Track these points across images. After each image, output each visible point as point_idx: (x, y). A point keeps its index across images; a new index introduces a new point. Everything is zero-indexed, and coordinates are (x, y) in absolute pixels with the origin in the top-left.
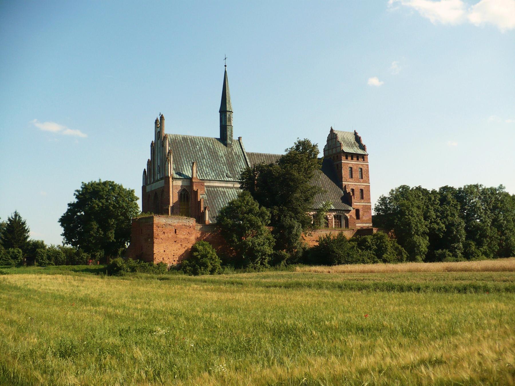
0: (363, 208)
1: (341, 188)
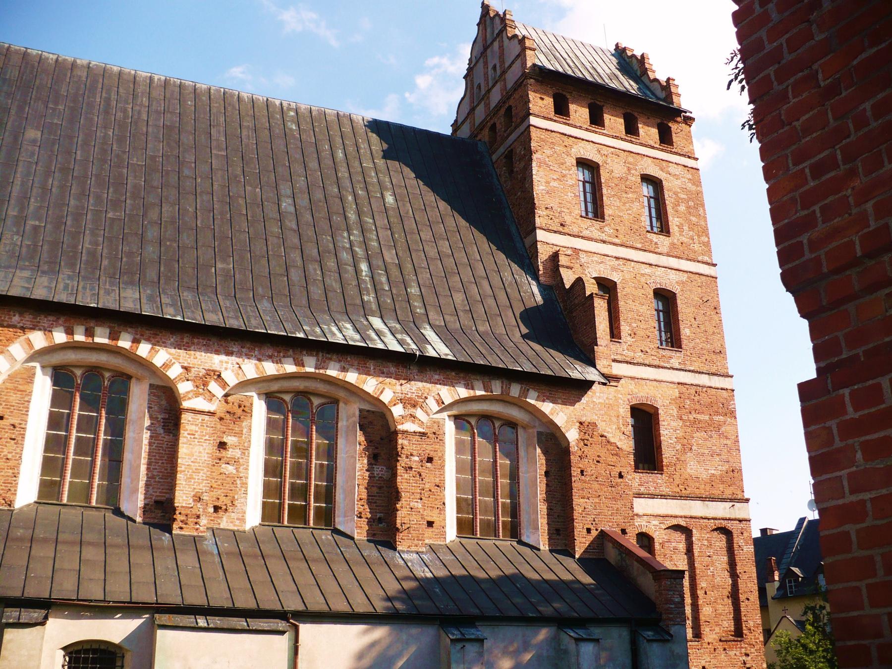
0: (679, 402)
1: (530, 268)
